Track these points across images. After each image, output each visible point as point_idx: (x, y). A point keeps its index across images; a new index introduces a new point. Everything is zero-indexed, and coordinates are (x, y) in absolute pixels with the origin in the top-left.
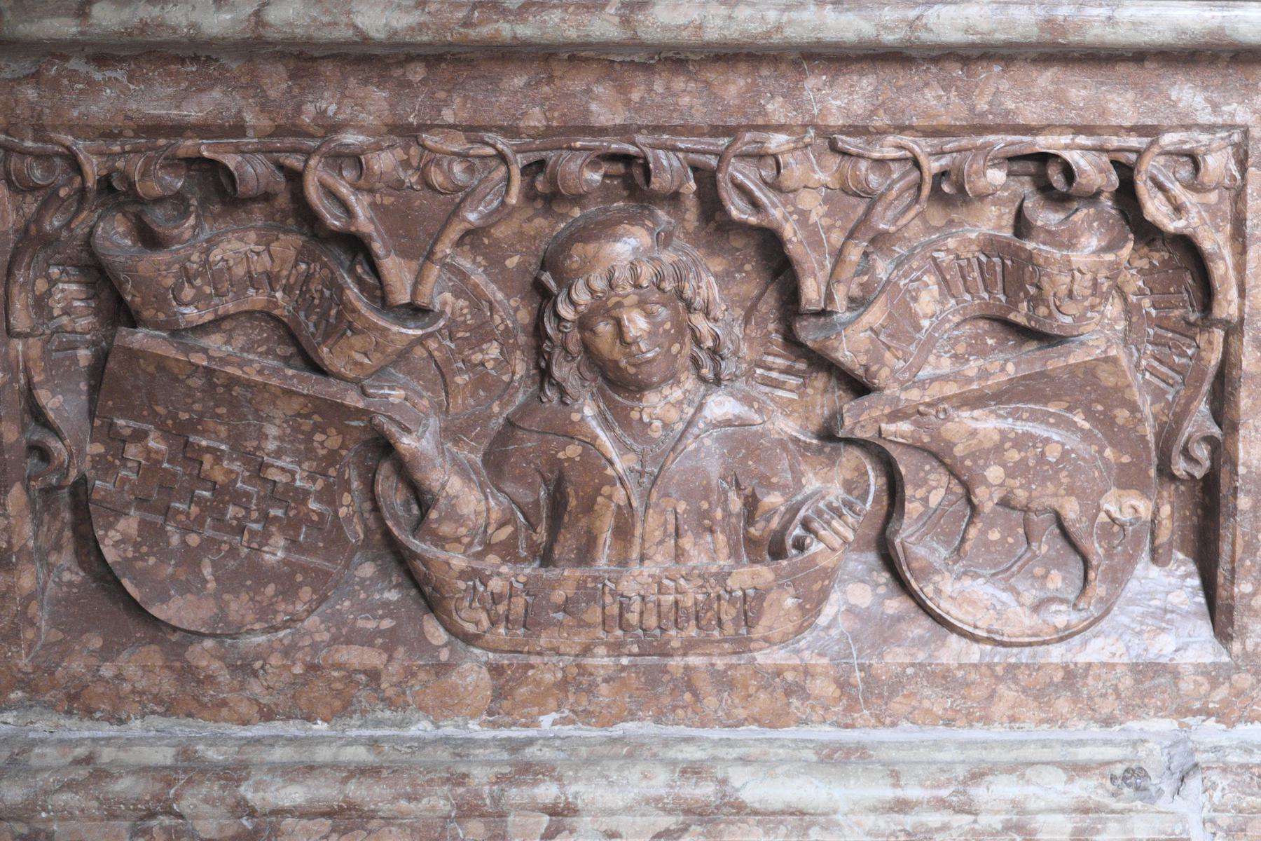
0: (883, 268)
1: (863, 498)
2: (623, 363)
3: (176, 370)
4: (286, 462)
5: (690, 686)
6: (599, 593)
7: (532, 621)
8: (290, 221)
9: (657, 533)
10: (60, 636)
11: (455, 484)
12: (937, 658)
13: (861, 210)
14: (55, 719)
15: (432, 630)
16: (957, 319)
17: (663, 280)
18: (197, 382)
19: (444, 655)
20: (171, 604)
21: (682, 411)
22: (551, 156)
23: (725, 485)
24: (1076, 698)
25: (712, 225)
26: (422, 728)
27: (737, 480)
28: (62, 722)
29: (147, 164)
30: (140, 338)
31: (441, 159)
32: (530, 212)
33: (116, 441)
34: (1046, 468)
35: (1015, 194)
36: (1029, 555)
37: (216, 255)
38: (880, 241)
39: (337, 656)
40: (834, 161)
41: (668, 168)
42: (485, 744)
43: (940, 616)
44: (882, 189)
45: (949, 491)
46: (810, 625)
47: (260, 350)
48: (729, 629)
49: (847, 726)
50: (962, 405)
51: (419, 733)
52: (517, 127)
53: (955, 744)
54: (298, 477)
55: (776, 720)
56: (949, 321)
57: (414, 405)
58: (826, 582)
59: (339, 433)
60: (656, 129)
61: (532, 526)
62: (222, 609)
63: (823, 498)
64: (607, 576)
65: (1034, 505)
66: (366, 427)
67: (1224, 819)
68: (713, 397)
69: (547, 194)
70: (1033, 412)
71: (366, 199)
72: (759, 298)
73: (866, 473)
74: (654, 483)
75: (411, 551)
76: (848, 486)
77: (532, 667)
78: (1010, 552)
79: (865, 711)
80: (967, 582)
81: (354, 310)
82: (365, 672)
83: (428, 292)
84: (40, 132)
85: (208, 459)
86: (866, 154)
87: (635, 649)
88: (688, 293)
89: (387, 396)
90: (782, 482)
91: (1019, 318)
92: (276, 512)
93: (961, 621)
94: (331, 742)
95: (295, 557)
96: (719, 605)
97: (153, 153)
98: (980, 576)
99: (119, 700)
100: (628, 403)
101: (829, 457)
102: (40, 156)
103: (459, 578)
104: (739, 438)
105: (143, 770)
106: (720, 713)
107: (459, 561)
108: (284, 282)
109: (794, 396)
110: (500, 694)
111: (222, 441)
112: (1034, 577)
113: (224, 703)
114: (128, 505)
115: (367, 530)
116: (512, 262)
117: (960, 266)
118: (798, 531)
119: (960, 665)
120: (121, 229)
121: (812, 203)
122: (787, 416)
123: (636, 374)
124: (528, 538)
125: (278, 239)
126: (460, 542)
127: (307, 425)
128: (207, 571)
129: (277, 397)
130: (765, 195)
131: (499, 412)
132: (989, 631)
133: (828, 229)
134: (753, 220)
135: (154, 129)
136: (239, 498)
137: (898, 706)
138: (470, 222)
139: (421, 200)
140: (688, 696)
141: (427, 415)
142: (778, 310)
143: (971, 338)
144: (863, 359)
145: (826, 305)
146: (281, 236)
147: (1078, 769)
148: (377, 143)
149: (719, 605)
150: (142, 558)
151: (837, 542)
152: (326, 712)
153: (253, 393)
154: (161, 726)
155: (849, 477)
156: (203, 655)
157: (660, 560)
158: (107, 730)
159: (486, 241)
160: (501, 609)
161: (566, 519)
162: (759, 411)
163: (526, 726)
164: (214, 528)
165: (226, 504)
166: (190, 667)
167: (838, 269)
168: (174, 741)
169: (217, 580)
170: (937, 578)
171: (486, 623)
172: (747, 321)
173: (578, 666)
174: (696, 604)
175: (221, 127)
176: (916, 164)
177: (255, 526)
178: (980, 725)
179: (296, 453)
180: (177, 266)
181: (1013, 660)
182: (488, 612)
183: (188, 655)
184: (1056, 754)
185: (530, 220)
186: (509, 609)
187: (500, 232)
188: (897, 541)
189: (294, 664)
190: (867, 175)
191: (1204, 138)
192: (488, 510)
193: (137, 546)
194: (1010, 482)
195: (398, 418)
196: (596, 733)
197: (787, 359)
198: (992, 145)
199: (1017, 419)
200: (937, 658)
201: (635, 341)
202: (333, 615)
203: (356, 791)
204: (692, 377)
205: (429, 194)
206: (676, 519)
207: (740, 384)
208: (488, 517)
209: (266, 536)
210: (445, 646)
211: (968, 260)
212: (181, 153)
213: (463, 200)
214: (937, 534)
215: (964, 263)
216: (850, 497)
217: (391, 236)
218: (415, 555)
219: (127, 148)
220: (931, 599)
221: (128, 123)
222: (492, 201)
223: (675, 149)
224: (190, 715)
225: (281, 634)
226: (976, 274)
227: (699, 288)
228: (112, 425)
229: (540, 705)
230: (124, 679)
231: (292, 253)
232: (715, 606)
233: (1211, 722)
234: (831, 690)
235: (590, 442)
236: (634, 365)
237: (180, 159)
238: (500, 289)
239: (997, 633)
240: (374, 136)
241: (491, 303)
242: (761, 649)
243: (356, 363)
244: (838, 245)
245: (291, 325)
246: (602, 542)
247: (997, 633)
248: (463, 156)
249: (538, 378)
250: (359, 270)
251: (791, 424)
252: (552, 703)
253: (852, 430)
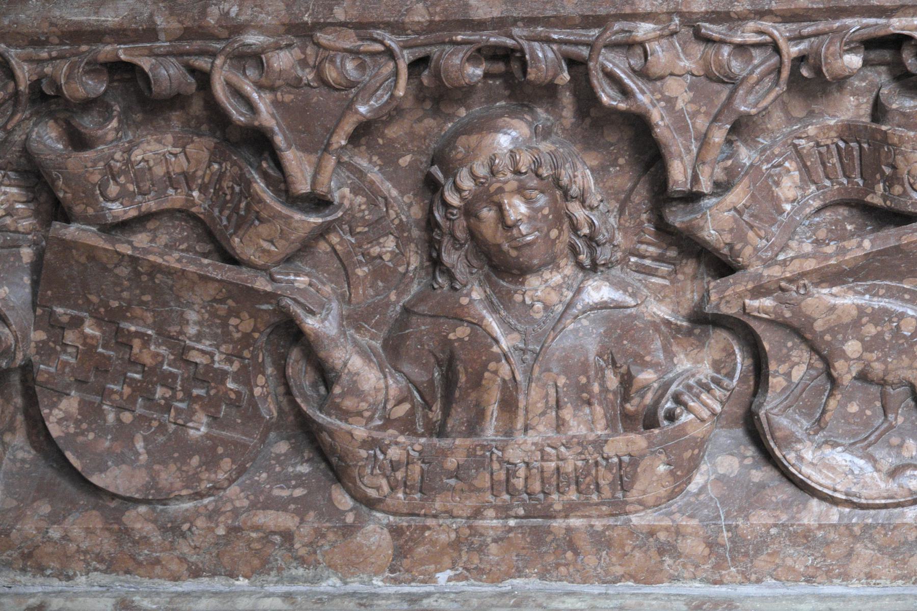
0: (745, 155)
1: (730, 375)
2: (506, 247)
3: (105, 260)
4: (205, 345)
6: (487, 460)
7: (427, 487)
8: (204, 127)
9: (539, 405)
10: (15, 503)
11: (356, 362)
12: (798, 520)
13: (724, 96)
14: (12, 575)
15: (340, 497)
16: (817, 204)
17: (540, 165)
18: (124, 271)
19: (350, 518)
20: (108, 473)
21: (562, 295)
22: (435, 51)
23: (602, 363)
25: (588, 121)
27: (613, 359)
28: (18, 578)
29: (72, 68)
30: (72, 231)
31: (335, 56)
32: (420, 113)
33: (55, 327)
34: (901, 342)
35: (872, 84)
36: (886, 425)
37: (137, 155)
38: (742, 128)
39: (256, 519)
40: (698, 49)
41: (544, 58)
42: (388, 597)
43: (802, 480)
44: (744, 74)
45: (810, 366)
46: (682, 491)
47: (181, 247)
48: (607, 493)
49: (715, 583)
50: (822, 282)
51: (330, 589)
52: (403, 23)
54: (216, 358)
55: (650, 577)
56: (810, 205)
57: (318, 291)
58: (696, 451)
59: (251, 317)
60: (531, 21)
61: (428, 405)
62: (153, 479)
63: (693, 375)
64: (494, 444)
65: (890, 378)
66: (274, 310)
68: (590, 282)
69: (439, 95)
70: (889, 288)
71: (268, 96)
72: (632, 190)
73: (734, 353)
74: (535, 360)
75: (318, 424)
77: (429, 528)
78: (867, 424)
79: (732, 569)
80: (827, 451)
81: (261, 201)
82: (280, 533)
83: (326, 182)
85: (137, 343)
86: (728, 39)
87: (521, 512)
88: (565, 180)
89: (292, 282)
90: (655, 360)
91: (875, 199)
93: (821, 485)
94: (251, 595)
95: (216, 432)
96: (597, 471)
97: (76, 59)
98: (839, 445)
99: (66, 558)
100: (512, 287)
101: (699, 338)
103: (361, 447)
104: (619, 326)
106: (599, 570)
107: (360, 432)
108: (200, 181)
109: (667, 282)
110: (401, 552)
111: (149, 327)
112: (890, 446)
113: (158, 561)
114: (68, 386)
115: (280, 411)
116: (405, 161)
117: (820, 153)
118: (669, 405)
119: (820, 525)
120: (53, 135)
121: (676, 88)
122: (660, 301)
123: (518, 257)
124: (425, 416)
125: (192, 142)
126: (362, 416)
127: (222, 309)
128: (140, 445)
129: (194, 283)
130: (634, 83)
131: (397, 301)
132: (847, 494)
133: (694, 115)
134: (623, 106)
135: (77, 35)
136: (167, 380)
137: (763, 564)
138: (362, 114)
139: (318, 96)
140: (569, 554)
141: (330, 300)
142: (650, 201)
143: (831, 224)
144: (728, 238)
145: (692, 186)
146: (196, 138)
148: (276, 43)
149: (597, 471)
150: (83, 433)
151: (705, 414)
152: (246, 570)
153: (172, 279)
154: (103, 582)
155: (717, 358)
156: (138, 519)
157: (543, 430)
158: (57, 584)
159: (381, 141)
160: (400, 475)
161: (457, 394)
162: (633, 295)
163: (424, 582)
164: (145, 407)
165: (154, 384)
166: (127, 529)
167: (703, 152)
168: (116, 594)
169: (148, 452)
170: (799, 446)
171: (386, 489)
172: (621, 212)
173: (470, 527)
174: (575, 470)
175: (136, 31)
176: (777, 49)
177: (180, 405)
178: (839, 581)
179: (215, 336)
180: (102, 164)
181: (870, 521)
182: (388, 478)
183: (124, 519)
185: (420, 120)
186: (407, 476)
187: (393, 131)
188: (762, 413)
189: (217, 526)
190: (729, 60)
192: (387, 387)
193: (78, 423)
194: (867, 356)
195: (302, 300)
196: (488, 589)
197: (659, 247)
198: (848, 28)
199: (874, 295)
200: (798, 520)
201: (516, 224)
202: (252, 485)
204: (571, 263)
205: (324, 90)
206: (557, 392)
207: (616, 271)
208: (387, 393)
209: (191, 413)
210: (351, 510)
211: (828, 146)
212: (102, 58)
213: (357, 95)
214: (799, 407)
215: (823, 150)
216: (719, 376)
217: (292, 131)
218: (321, 428)
219: (54, 54)
220: (793, 466)
221: (54, 29)
222: (382, 96)
223: (549, 41)
224: (127, 572)
225: (206, 501)
226: (835, 160)
227: (575, 176)
228: (52, 313)
229: (436, 563)
230: (70, 540)
231: (205, 155)
232: (593, 472)
235: (477, 325)
236: (516, 248)
237: (101, 64)
238: (394, 186)
239: (855, 495)
240: (273, 36)
241: (385, 198)
242: (636, 512)
243: (264, 251)
244: (703, 130)
245: (207, 221)
246: (489, 413)
247: (855, 495)
248: (354, 53)
249: (431, 270)
250: (264, 165)
251: (663, 308)
252: (447, 561)
253: (718, 306)
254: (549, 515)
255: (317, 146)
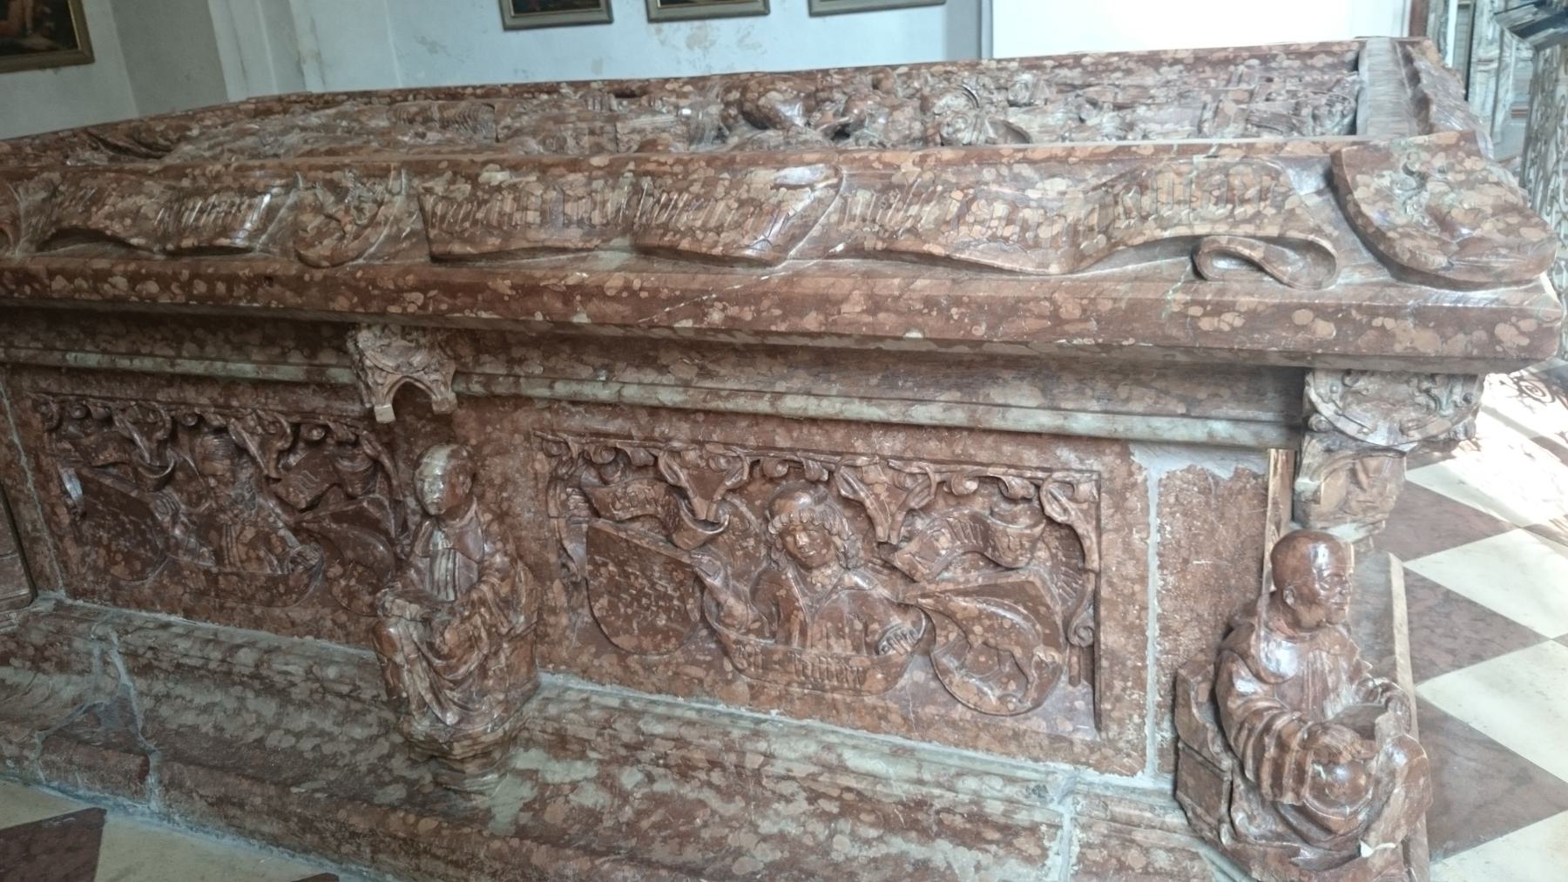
5: (835, 707)
7: (766, 667)
19: (730, 676)
24: (1020, 746)
26: (721, 707)
33: (597, 565)
37: (629, 490)
42: (746, 718)
53: (956, 756)
55: (876, 730)
67: (1083, 820)
76: (914, 624)
84: (554, 432)
92: (661, 603)
99: (601, 676)
102: (555, 442)
105: (605, 708)
116: (758, 503)
135: (598, 434)
136: (647, 596)
147: (1011, 780)
156: (633, 661)
158: (598, 688)
184: (1001, 771)
191: (1078, 476)
196: (796, 722)
203: (685, 732)
233: (1091, 770)
234: (900, 720)
235: (789, 590)
248: (724, 456)
254: (824, 691)
255: (708, 497)
